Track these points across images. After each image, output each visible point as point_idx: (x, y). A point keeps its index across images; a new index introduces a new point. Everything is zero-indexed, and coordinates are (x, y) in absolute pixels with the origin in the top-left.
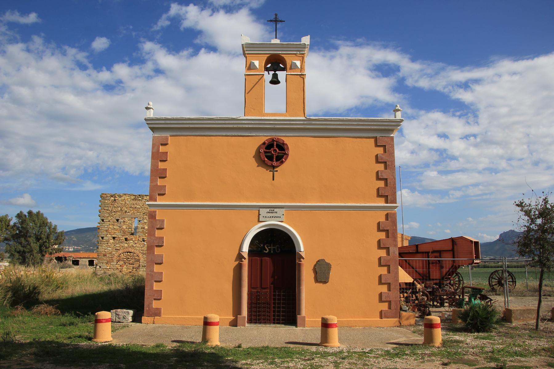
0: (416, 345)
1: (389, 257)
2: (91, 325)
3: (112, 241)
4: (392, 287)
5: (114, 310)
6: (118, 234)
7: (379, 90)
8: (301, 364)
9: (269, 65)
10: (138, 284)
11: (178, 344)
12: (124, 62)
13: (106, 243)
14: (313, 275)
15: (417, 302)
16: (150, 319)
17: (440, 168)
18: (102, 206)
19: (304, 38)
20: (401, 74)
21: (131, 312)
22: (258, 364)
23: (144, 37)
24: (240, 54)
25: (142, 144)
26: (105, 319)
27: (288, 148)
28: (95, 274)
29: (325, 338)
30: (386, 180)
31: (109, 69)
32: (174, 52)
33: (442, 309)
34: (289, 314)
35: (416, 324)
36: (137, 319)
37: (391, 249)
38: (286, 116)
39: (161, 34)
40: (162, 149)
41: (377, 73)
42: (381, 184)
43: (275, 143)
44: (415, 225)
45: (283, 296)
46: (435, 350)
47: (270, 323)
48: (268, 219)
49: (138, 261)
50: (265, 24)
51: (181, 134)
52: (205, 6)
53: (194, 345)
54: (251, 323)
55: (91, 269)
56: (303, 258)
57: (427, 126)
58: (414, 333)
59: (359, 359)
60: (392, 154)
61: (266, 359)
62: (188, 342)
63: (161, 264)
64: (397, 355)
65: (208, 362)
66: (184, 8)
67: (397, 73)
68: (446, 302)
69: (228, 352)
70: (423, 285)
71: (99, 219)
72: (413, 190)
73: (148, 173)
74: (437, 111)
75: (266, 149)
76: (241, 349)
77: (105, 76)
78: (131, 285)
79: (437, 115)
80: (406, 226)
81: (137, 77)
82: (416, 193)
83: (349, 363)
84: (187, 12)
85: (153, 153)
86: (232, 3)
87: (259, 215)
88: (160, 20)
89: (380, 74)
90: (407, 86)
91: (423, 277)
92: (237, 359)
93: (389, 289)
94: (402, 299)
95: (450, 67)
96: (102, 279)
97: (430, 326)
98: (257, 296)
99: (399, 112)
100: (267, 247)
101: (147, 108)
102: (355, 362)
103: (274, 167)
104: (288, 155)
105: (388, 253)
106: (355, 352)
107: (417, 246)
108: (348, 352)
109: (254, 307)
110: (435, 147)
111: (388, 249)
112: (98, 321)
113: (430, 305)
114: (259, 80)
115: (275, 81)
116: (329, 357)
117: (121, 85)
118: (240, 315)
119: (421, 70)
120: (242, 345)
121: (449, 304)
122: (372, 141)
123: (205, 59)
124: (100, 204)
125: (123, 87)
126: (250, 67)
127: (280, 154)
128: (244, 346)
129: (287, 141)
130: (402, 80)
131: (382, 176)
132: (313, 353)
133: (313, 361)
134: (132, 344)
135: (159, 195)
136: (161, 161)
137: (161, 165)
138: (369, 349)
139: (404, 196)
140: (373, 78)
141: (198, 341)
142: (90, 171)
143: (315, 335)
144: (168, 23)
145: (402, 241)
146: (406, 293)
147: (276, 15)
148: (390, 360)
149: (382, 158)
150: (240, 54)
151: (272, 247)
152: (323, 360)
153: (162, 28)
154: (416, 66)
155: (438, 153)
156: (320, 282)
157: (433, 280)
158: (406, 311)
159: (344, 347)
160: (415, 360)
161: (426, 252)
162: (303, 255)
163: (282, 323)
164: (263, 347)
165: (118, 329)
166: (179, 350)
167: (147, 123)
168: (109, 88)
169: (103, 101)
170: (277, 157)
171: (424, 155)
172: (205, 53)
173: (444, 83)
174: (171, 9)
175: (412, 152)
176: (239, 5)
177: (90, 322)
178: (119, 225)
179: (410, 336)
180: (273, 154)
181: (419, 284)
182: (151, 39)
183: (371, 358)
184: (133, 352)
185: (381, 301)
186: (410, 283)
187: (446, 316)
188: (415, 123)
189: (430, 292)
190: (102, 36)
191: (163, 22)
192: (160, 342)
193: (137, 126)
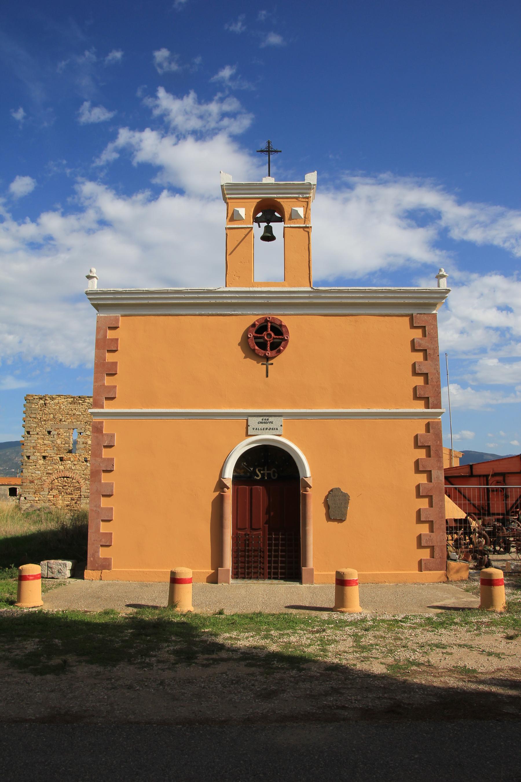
0: (469, 609)
1: (431, 485)
2: (13, 582)
3: (41, 462)
4: (435, 526)
5: (46, 562)
6: (50, 452)
7: (412, 245)
8: (307, 638)
9: (260, 215)
10: (78, 523)
11: (135, 610)
12: (55, 210)
13: (33, 464)
14: (323, 510)
15: (471, 546)
16: (96, 574)
17: (502, 354)
18: (28, 413)
19: (308, 175)
20: (442, 223)
21: (69, 564)
22: (247, 638)
23: (83, 176)
24: (217, 198)
25: (75, 337)
26: (32, 576)
27: (287, 332)
28: (18, 507)
29: (341, 601)
30: (426, 375)
31: (34, 220)
32: (125, 196)
33: (507, 556)
34: (291, 568)
35: (470, 578)
36: (77, 573)
37: (434, 473)
38: (284, 286)
39: (106, 171)
40: (111, 335)
41: (409, 221)
42: (420, 381)
43: (269, 324)
44: (468, 434)
45: (283, 539)
46: (496, 617)
47: (264, 578)
48: (259, 432)
49: (79, 489)
50: (251, 155)
51: (136, 313)
52: (166, 133)
53: (157, 612)
54: (237, 578)
55: (12, 501)
56: (310, 487)
57: (482, 295)
58: (467, 591)
59: (389, 630)
60: (434, 338)
61: (258, 631)
62: (148, 607)
63: (110, 496)
64: (442, 624)
65: (176, 635)
66: (137, 135)
67: (438, 222)
68: (513, 547)
69: (204, 620)
70: (480, 522)
71: (23, 432)
72: (464, 385)
73: (91, 366)
74: (496, 274)
75: (256, 333)
76: (223, 616)
77: (29, 230)
78: (68, 523)
79: (495, 280)
80: (456, 436)
81: (73, 231)
82: (469, 389)
83: (374, 637)
84: (141, 141)
85: (97, 340)
86: (205, 126)
87: (248, 426)
88: (104, 152)
89: (413, 223)
90: (452, 240)
91: (481, 511)
92: (218, 632)
93: (431, 530)
94: (451, 542)
95: (512, 212)
96: (27, 515)
97: (489, 583)
98: (245, 540)
99: (445, 279)
100: (259, 471)
101: (89, 277)
102: (383, 634)
103: (268, 359)
104: (287, 341)
105: (430, 479)
106: (383, 621)
107: (471, 467)
108: (374, 620)
109: (241, 556)
110: (494, 325)
111: (429, 473)
112: (22, 578)
113: (490, 551)
114: (246, 236)
115: (268, 237)
116: (347, 628)
117: (52, 242)
118: (222, 567)
119: (472, 217)
120: (225, 611)
121: (517, 549)
122: (407, 319)
123: (168, 205)
124: (24, 409)
125: (55, 245)
126: (233, 217)
127: (276, 340)
128: (228, 612)
129: (285, 321)
130: (444, 232)
131: (420, 369)
132: (324, 622)
133: (324, 634)
134: (71, 609)
135: (107, 399)
136: (109, 351)
137: (110, 358)
138: (402, 616)
139: (452, 394)
140: (405, 228)
141: (162, 605)
142: (9, 362)
143: (328, 598)
144: (115, 156)
145: (451, 459)
146: (457, 533)
147: (269, 143)
148: (433, 631)
149: (420, 345)
150: (217, 198)
151: (266, 472)
152: (338, 632)
153: (108, 163)
154: (465, 211)
155: (499, 333)
156: (335, 520)
157: (494, 514)
158: (455, 560)
159: (367, 613)
160: (467, 631)
161: (484, 476)
162: (310, 482)
163: (281, 579)
164: (254, 614)
165: (51, 588)
166: (136, 618)
167: (89, 299)
168: (35, 246)
169: (26, 265)
170: (271, 344)
171: (478, 336)
172: (168, 197)
173: (504, 235)
174: (119, 136)
175: (462, 332)
176: (213, 129)
177: (12, 577)
178: (51, 439)
179: (461, 596)
180: (266, 340)
181: (474, 520)
182: (93, 178)
183: (405, 628)
184: (71, 621)
185: (420, 546)
186: (461, 520)
187: (513, 567)
188: (464, 291)
189: (489, 533)
190: (24, 175)
191: (109, 155)
192: (109, 606)
193: (73, 299)
